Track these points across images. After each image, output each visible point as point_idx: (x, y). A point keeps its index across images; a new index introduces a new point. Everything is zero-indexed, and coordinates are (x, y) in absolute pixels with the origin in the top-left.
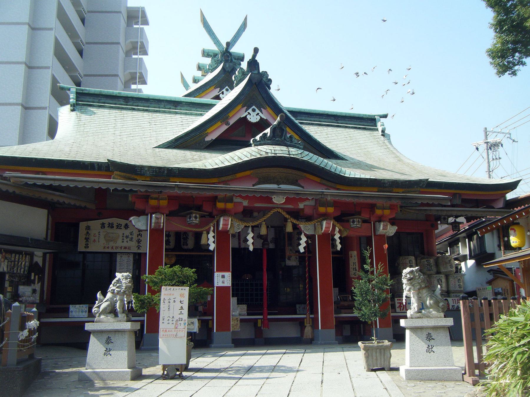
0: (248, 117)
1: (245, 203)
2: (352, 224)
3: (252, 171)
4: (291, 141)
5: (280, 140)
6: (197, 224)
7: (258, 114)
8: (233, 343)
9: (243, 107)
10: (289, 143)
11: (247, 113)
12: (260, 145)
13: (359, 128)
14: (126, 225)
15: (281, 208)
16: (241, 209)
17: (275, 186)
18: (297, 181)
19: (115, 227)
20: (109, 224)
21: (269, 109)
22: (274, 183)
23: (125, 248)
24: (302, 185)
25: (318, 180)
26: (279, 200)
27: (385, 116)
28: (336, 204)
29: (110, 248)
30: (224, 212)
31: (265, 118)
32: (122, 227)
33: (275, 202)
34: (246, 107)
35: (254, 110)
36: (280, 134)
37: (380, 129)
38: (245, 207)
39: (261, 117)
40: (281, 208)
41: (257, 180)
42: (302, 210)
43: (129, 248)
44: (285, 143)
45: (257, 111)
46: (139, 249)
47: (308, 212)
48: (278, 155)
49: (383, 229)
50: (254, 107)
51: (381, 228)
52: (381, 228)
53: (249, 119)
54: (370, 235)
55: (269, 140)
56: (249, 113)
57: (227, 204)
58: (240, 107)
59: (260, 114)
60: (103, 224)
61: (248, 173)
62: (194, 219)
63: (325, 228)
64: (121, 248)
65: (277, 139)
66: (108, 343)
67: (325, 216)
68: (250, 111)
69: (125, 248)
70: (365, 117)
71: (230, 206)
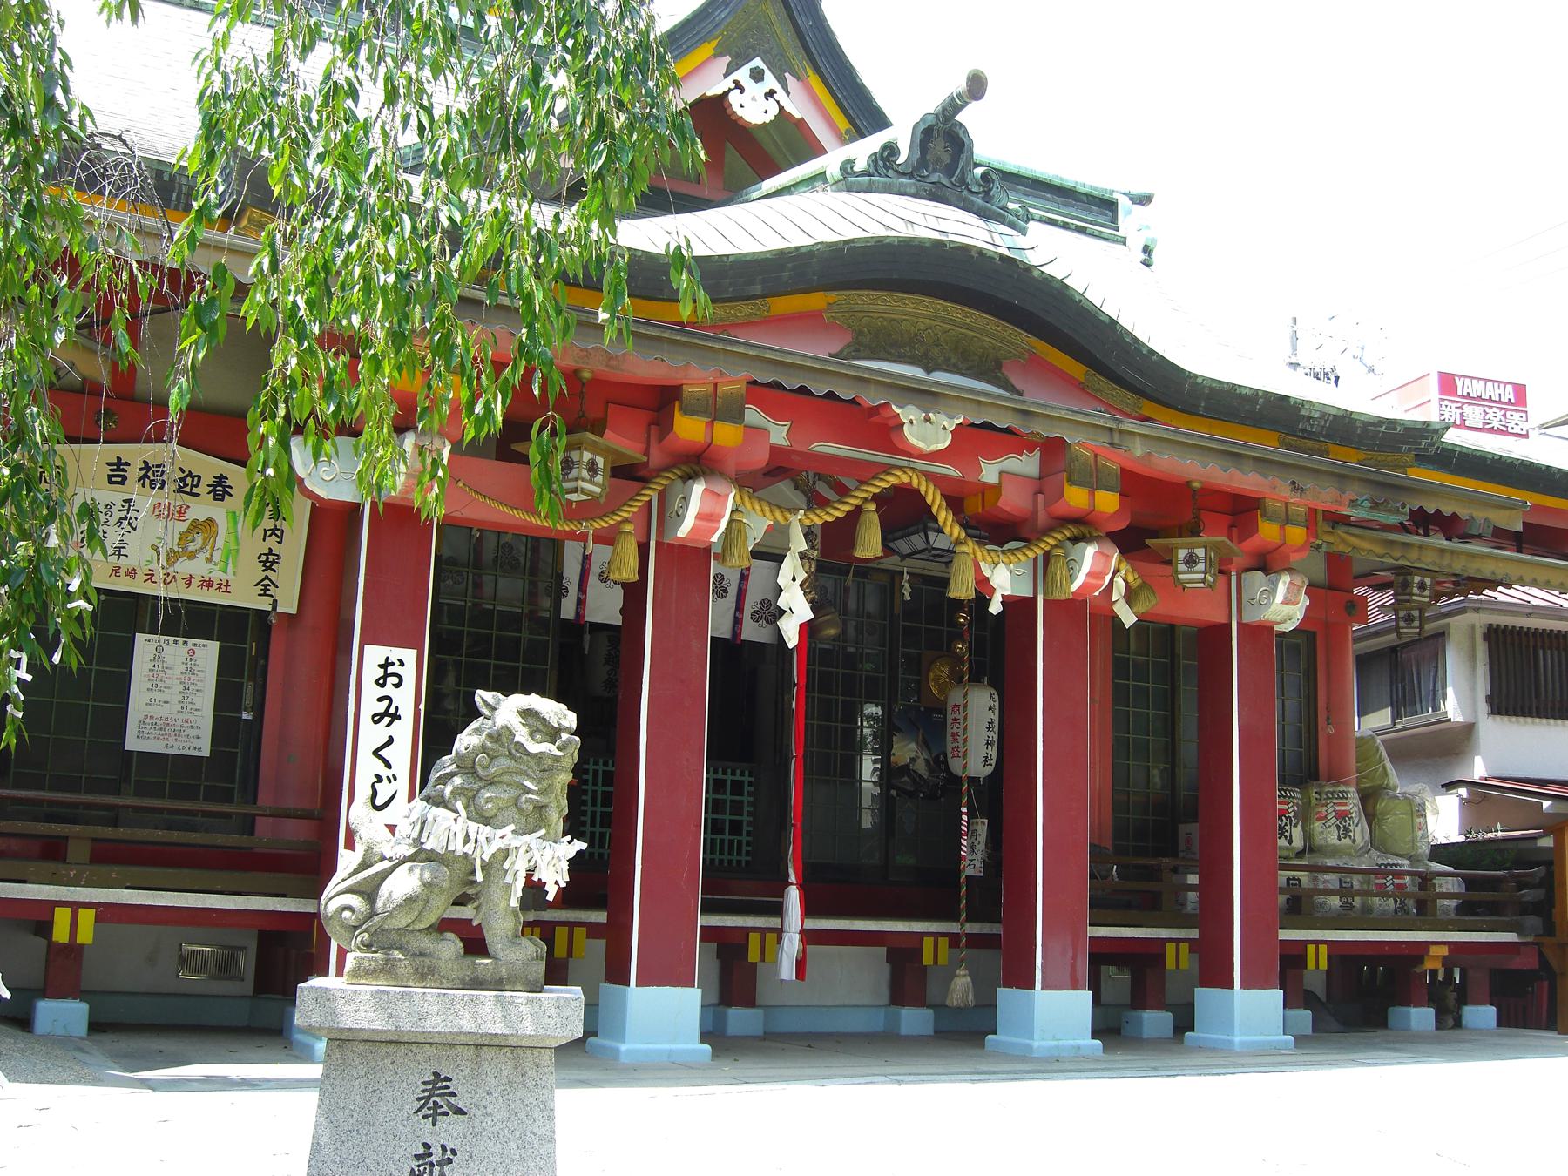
0: (734, 98)
1: (779, 434)
2: (1182, 567)
3: (832, 296)
4: (987, 197)
5: (945, 181)
6: (595, 499)
7: (770, 94)
8: (702, 1041)
9: (718, 54)
10: (978, 200)
11: (728, 83)
12: (870, 189)
13: (1065, 226)
14: (221, 480)
15: (930, 476)
16: (761, 458)
17: (916, 372)
18: (999, 365)
19: (170, 487)
20: (146, 467)
21: (814, 81)
22: (911, 361)
23: (207, 583)
24: (1019, 386)
25: (1077, 370)
26: (927, 432)
27: (1144, 200)
28: (1133, 484)
29: (140, 577)
30: (698, 463)
31: (798, 116)
32: (203, 489)
33: (914, 442)
34: (728, 59)
35: (757, 76)
36: (946, 159)
37: (1135, 244)
38: (775, 450)
39: (781, 108)
40: (930, 476)
41: (848, 339)
42: (996, 489)
43: (225, 587)
44: (965, 200)
45: (770, 81)
46: (265, 593)
47: (1013, 501)
48: (951, 238)
49: (1286, 602)
50: (757, 62)
51: (1279, 597)
52: (1279, 597)
53: (736, 107)
54: (1223, 620)
55: (903, 175)
56: (738, 85)
57: (718, 425)
58: (707, 49)
59: (780, 95)
60: (119, 465)
61: (816, 301)
62: (585, 474)
63: (1089, 574)
64: (189, 580)
65: (935, 177)
66: (436, 1114)
67: (1083, 527)
68: (743, 74)
69: (207, 583)
70: (1082, 190)
71: (726, 435)
